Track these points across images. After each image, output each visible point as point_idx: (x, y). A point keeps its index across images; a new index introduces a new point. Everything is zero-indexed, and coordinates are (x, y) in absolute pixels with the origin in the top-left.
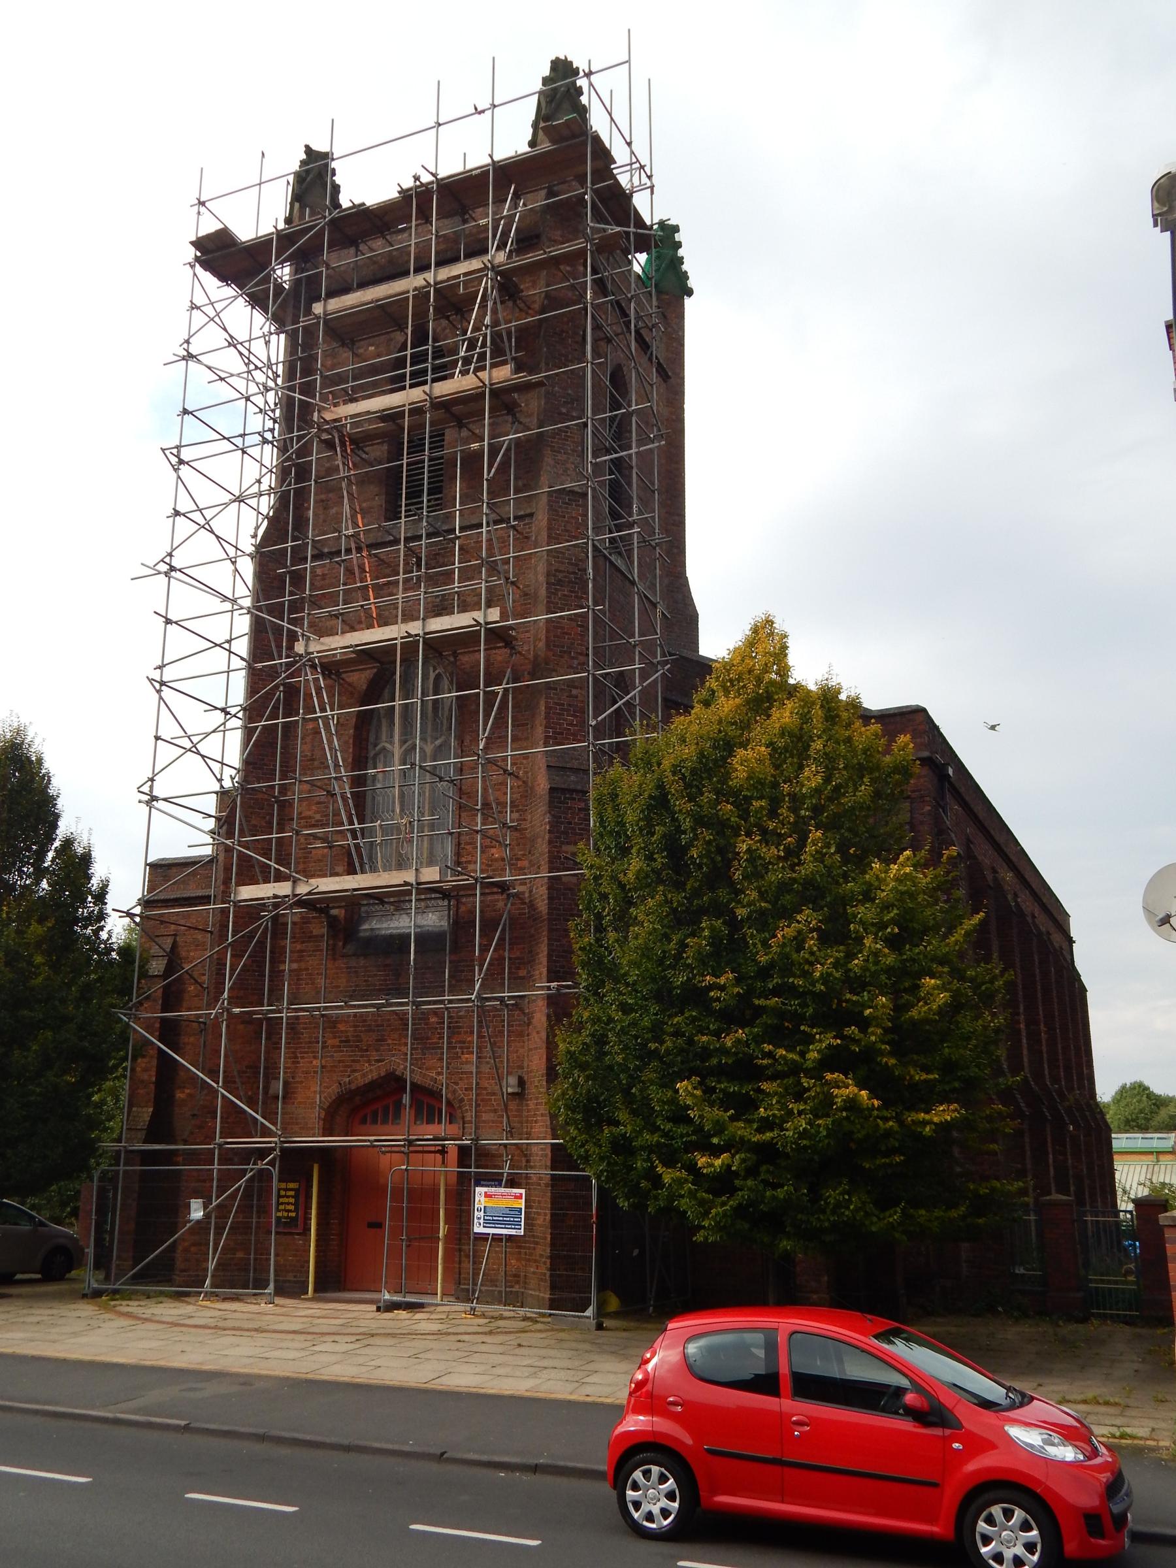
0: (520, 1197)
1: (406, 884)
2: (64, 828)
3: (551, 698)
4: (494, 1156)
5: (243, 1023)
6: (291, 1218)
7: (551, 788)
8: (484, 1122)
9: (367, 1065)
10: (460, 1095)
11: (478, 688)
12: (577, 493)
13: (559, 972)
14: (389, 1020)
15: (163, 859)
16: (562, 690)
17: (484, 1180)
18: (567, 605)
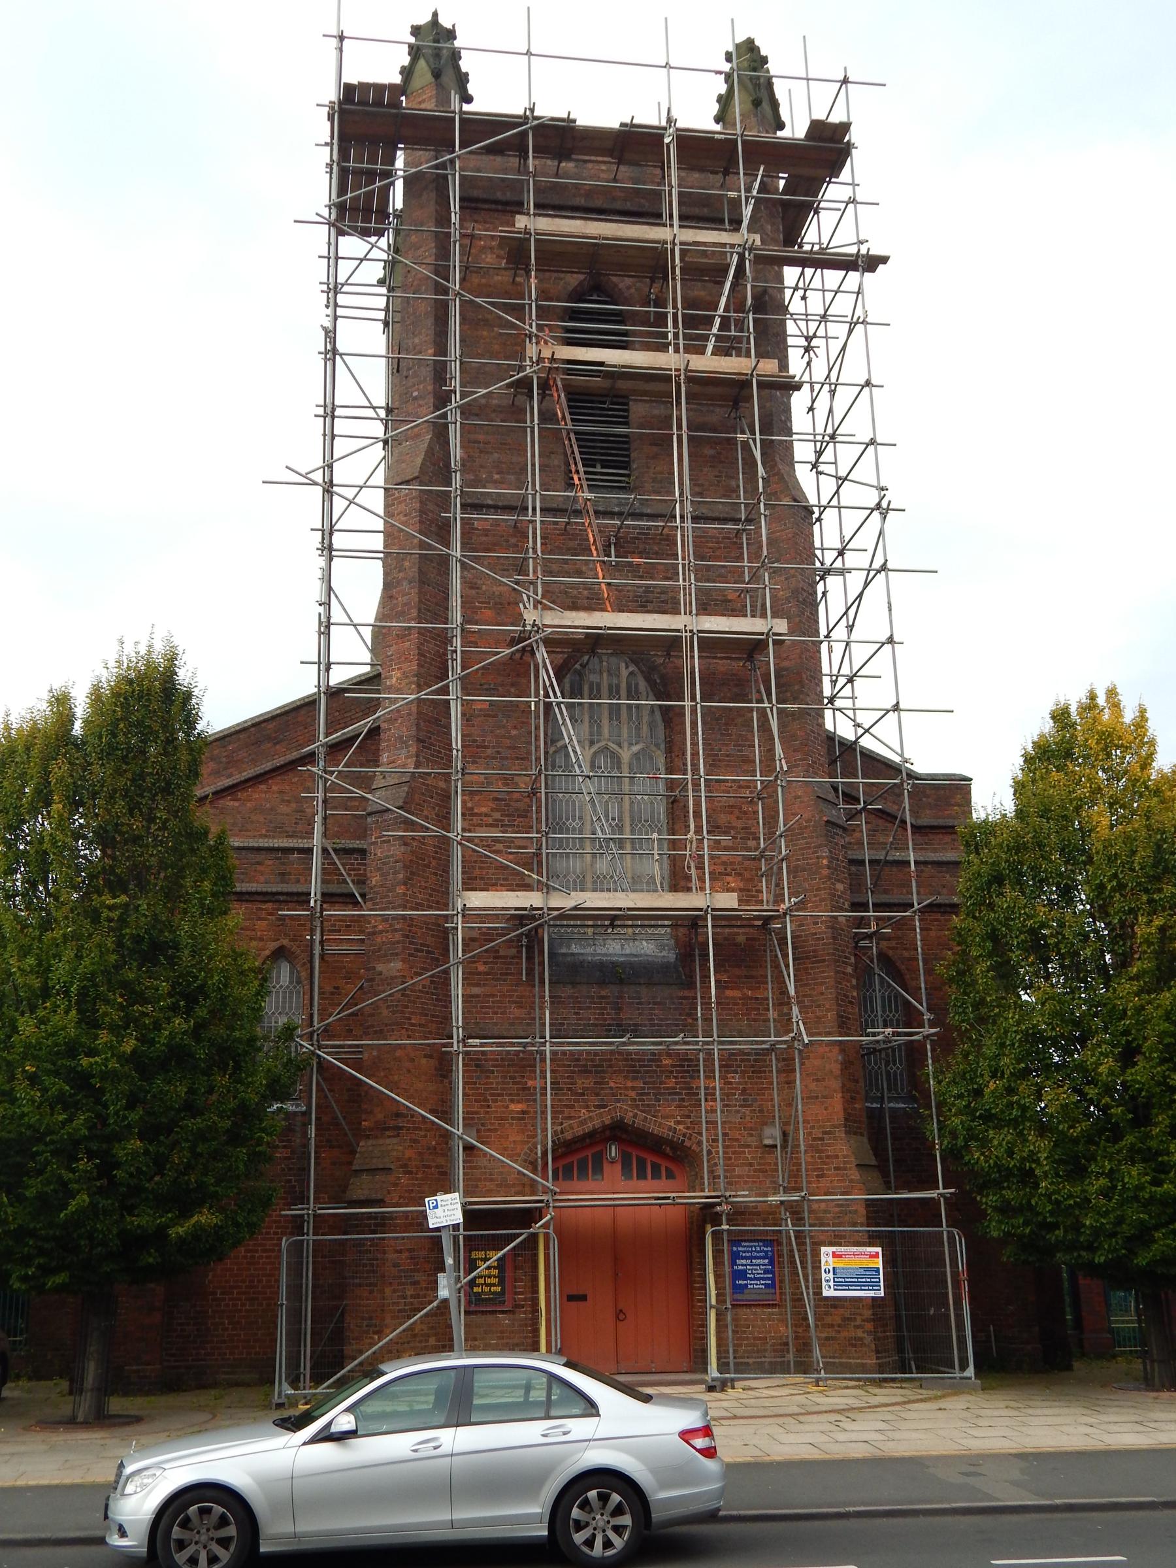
0: (876, 1255)
5: (425, 1056)
6: (495, 1293)
14: (610, 1060)
17: (745, 1241)
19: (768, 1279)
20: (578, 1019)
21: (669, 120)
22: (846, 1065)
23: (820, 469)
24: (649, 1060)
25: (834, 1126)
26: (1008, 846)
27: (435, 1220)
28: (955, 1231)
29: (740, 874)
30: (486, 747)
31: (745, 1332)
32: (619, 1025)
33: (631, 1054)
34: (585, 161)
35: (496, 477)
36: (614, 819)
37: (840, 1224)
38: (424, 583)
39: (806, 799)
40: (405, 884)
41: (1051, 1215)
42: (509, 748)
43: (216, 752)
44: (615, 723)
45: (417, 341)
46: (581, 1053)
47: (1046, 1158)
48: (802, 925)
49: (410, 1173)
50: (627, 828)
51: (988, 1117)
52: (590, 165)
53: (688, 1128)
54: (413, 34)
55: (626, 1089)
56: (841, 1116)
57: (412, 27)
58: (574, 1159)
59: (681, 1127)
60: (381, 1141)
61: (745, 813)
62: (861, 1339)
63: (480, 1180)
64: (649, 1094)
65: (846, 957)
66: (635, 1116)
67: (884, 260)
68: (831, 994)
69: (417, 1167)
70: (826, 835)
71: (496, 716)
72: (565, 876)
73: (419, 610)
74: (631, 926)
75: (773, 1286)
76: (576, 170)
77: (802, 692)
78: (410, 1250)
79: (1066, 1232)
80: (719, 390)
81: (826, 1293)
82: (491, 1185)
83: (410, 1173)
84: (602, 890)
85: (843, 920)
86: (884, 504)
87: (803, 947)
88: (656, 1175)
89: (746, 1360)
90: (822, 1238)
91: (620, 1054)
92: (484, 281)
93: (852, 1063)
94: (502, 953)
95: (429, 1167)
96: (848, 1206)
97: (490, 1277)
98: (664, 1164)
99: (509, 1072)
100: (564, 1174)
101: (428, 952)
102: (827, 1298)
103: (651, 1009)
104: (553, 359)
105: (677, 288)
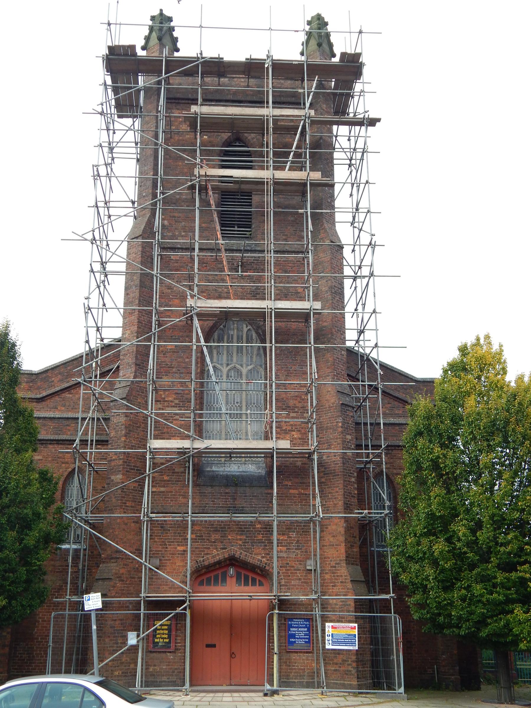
0: (355, 628)
5: (134, 522)
6: (165, 642)
14: (229, 525)
19: (306, 638)
20: (214, 504)
21: (268, 57)
22: (348, 529)
23: (355, 225)
24: (249, 525)
25: (341, 561)
26: (423, 416)
27: (88, 607)
28: (397, 616)
29: (299, 431)
30: (173, 368)
31: (294, 666)
32: (234, 507)
34: (234, 78)
35: (183, 234)
36: (237, 403)
37: (342, 611)
38: (142, 287)
39: (332, 393)
40: (125, 436)
41: (437, 609)
42: (184, 368)
43: (62, 370)
44: (240, 354)
45: (146, 168)
46: (214, 521)
47: (433, 579)
48: (329, 457)
49: (123, 581)
50: (244, 408)
51: (410, 558)
52: (236, 79)
53: (268, 560)
54: (151, 20)
55: (237, 540)
56: (344, 556)
57: (151, 16)
58: (212, 575)
59: (264, 559)
60: (109, 565)
61: (303, 400)
62: (350, 671)
63: (161, 585)
64: (248, 542)
65: (351, 473)
66: (241, 553)
67: (379, 120)
68: (341, 492)
69: (127, 578)
70: (341, 411)
71: (178, 352)
72: (211, 432)
73: (140, 301)
74: (245, 457)
75: (309, 642)
76: (228, 82)
77: (332, 338)
78: (121, 620)
79: (444, 618)
80: (293, 188)
81: (328, 647)
82: (166, 588)
83: (123, 581)
84: (237, 439)
85: (351, 454)
86: (373, 243)
87: (330, 468)
88: (254, 583)
89: (294, 680)
90: (334, 618)
91: (234, 521)
92: (181, 138)
93: (352, 528)
94: (176, 470)
95: (134, 578)
96: (346, 602)
98: (258, 578)
99: (178, 530)
100: (206, 583)
101: (137, 470)
102: (328, 650)
103: (251, 499)
104: (206, 176)
105: (270, 138)
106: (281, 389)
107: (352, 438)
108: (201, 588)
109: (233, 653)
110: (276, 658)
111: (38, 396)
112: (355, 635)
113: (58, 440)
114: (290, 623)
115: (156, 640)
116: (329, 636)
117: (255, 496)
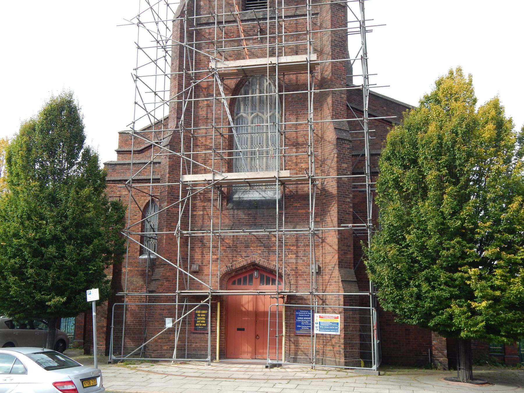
0: (337, 318)
1: (275, 177)
2: (87, 143)
3: (334, 98)
4: (305, 299)
6: (204, 326)
7: (338, 139)
8: (301, 284)
9: (240, 258)
10: (288, 273)
11: (307, 90)
12: (342, 5)
13: (342, 219)
14: (251, 239)
15: (111, 161)
16: (338, 94)
18: (338, 56)
33: (260, 236)
49: (168, 281)
58: (242, 277)
65: (346, 195)
66: (260, 260)
74: (265, 185)
78: (168, 309)
85: (346, 179)
97: (202, 320)
106: (292, 129)
107: (348, 166)
108: (234, 286)
109: (257, 335)
110: (284, 338)
111: (139, 149)
112: (338, 323)
113: (138, 180)
114: (297, 313)
115: (197, 325)
116: (317, 323)
117: (271, 216)
